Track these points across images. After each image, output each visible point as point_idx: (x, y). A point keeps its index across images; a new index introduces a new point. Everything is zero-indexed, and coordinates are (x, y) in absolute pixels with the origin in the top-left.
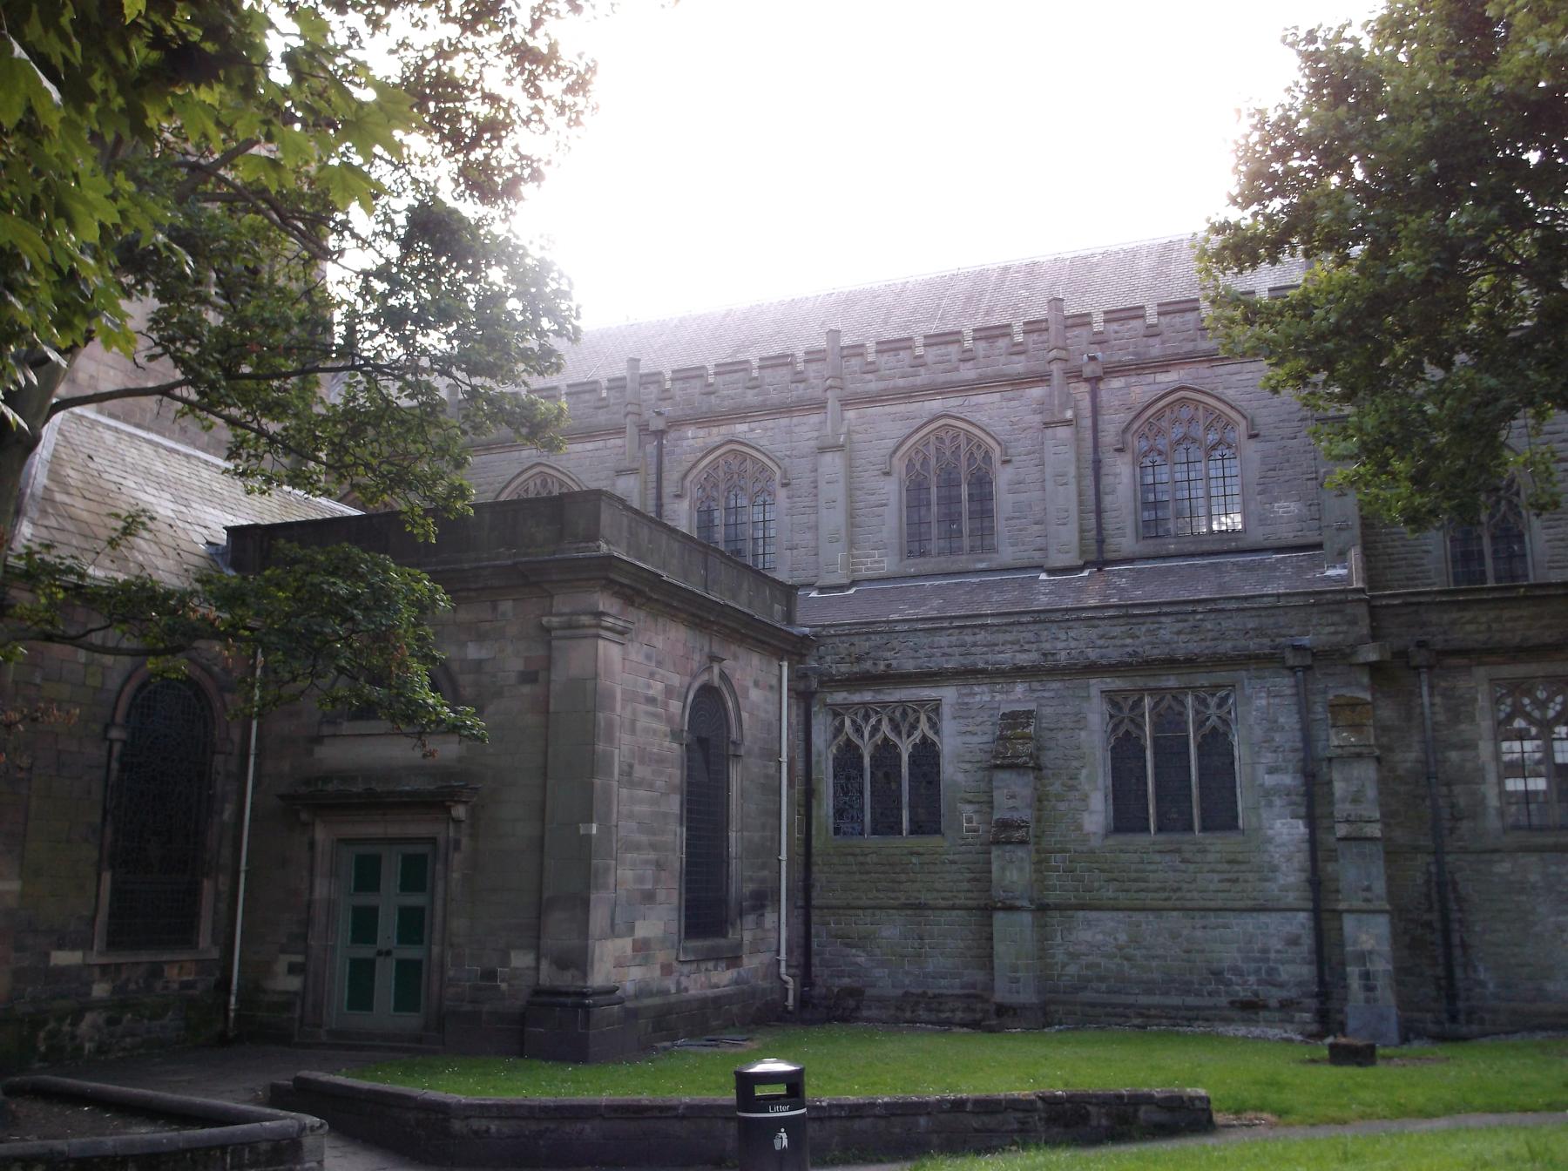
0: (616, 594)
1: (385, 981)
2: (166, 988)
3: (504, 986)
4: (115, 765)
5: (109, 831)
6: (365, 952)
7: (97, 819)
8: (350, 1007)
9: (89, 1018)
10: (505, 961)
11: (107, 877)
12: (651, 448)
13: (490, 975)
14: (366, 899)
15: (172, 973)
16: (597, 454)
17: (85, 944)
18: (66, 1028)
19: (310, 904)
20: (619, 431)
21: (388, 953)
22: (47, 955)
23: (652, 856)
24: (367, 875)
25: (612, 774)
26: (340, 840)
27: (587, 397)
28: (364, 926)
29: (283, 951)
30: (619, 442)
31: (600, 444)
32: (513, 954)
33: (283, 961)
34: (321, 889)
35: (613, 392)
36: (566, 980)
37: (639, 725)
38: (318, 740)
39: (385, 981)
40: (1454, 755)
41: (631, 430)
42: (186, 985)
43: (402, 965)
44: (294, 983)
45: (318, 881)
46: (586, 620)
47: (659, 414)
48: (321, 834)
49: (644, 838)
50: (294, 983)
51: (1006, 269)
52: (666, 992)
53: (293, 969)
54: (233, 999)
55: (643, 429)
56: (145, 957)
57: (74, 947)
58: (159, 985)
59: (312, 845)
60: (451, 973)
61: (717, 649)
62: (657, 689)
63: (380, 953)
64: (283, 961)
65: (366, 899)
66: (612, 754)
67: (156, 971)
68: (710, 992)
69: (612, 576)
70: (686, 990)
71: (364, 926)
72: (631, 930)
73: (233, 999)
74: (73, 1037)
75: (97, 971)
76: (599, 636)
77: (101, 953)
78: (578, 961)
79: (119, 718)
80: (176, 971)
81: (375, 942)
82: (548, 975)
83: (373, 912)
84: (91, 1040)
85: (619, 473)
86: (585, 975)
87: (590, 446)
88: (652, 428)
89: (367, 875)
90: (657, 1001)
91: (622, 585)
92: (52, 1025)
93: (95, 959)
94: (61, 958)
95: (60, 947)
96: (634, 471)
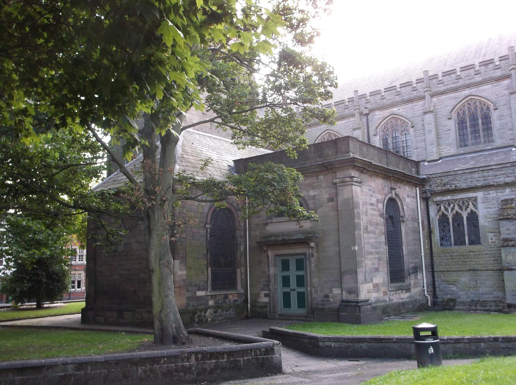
0: (357, 170)
2: (229, 302)
3: (331, 300)
4: (209, 236)
5: (209, 256)
6: (287, 290)
7: (206, 252)
9: (209, 311)
10: (331, 292)
11: (210, 269)
12: (364, 120)
13: (327, 296)
14: (286, 273)
15: (231, 297)
16: (346, 124)
17: (206, 289)
18: (203, 314)
19: (269, 275)
20: (353, 115)
21: (294, 290)
22: (196, 293)
23: (377, 256)
24: (285, 266)
25: (360, 230)
27: (341, 105)
28: (286, 281)
29: (262, 290)
30: (353, 119)
31: (347, 121)
32: (333, 289)
34: (272, 270)
35: (350, 103)
36: (352, 297)
37: (368, 213)
38: (266, 224)
41: (357, 115)
42: (235, 301)
44: (266, 300)
46: (347, 179)
47: (366, 108)
49: (373, 250)
50: (266, 300)
52: (385, 301)
54: (249, 305)
55: (361, 114)
56: (223, 292)
57: (203, 290)
58: (227, 301)
59: (268, 257)
60: (314, 296)
61: (393, 185)
62: (374, 200)
63: (291, 290)
64: (263, 293)
65: (286, 273)
66: (360, 223)
67: (226, 297)
68: (400, 301)
69: (355, 164)
70: (392, 300)
71: (286, 281)
72: (372, 281)
73: (249, 305)
74: (205, 317)
75: (210, 297)
76: (352, 184)
77: (210, 292)
78: (355, 291)
79: (209, 222)
80: (232, 296)
82: (346, 296)
84: (210, 318)
85: (354, 129)
86: (358, 296)
87: (343, 122)
88: (364, 113)
89: (285, 266)
90: (383, 304)
91: (359, 167)
92: (199, 313)
93: (209, 293)
94: (200, 293)
95: (199, 290)
96: (359, 128)
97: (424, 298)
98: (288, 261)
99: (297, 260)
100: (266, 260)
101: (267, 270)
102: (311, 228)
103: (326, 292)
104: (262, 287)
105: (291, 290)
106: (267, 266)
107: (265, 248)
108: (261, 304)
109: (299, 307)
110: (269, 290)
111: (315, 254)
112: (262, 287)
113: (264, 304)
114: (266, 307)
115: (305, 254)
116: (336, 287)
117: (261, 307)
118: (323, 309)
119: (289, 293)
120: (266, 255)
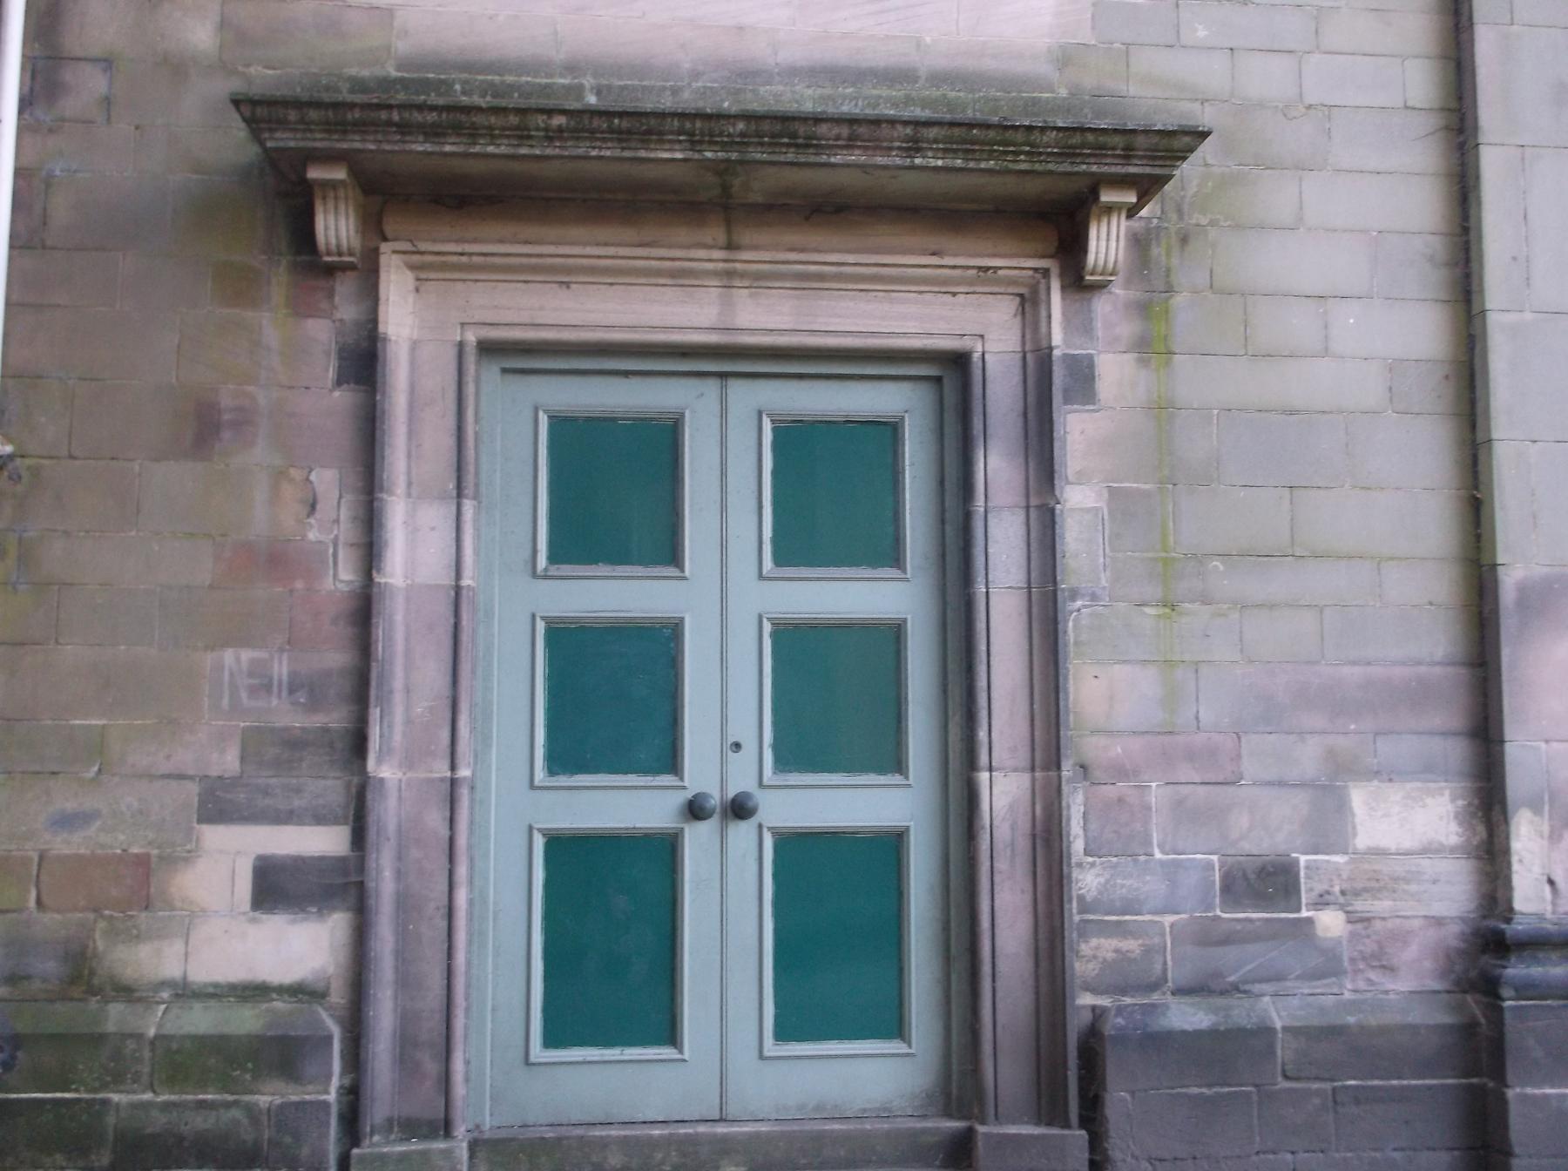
1: (726, 914)
3: (1330, 923)
8: (552, 1039)
10: (1329, 825)
13: (1269, 882)
14: (614, 595)
19: (364, 610)
21: (739, 809)
24: (614, 493)
26: (489, 349)
28: (612, 697)
29: (219, 806)
32: (1358, 796)
33: (226, 857)
34: (415, 547)
39: (726, 914)
40: (116, 1010)
43: (801, 853)
44: (304, 948)
45: (397, 513)
48: (405, 314)
50: (304, 948)
51: (807, 219)
53: (275, 887)
59: (363, 362)
63: (695, 810)
64: (226, 857)
65: (614, 595)
71: (612, 697)
81: (671, 762)
83: (660, 644)
89: (614, 493)
97: (1104, 851)
98: (661, 442)
99: (797, 442)
100: (334, 403)
101: (329, 529)
102: (1065, 58)
103: (1265, 825)
104: (228, 761)
105: (695, 810)
106: (328, 481)
107: (336, 227)
108: (199, 1020)
109: (797, 1022)
110: (359, 818)
111: (1115, 371)
112: (228, 761)
113: (246, 1021)
114: (283, 1054)
115: (953, 371)
116: (1386, 774)
117: (184, 1061)
118: (1232, 1052)
119: (662, 851)
120: (321, 335)
